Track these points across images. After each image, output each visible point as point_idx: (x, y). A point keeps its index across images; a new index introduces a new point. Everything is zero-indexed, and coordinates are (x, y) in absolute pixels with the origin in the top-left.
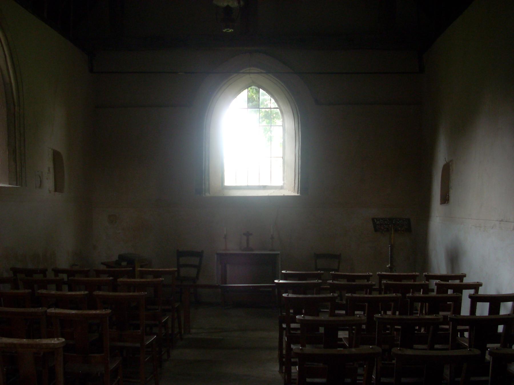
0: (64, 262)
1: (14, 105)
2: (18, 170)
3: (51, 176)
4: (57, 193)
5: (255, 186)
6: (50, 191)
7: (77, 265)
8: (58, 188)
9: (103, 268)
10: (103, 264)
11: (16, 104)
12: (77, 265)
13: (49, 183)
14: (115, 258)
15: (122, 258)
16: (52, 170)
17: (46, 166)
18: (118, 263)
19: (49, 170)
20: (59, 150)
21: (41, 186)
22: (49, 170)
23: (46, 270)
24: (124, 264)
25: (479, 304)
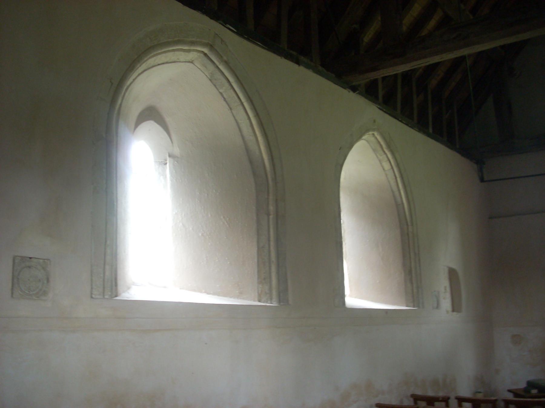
0: (465, 391)
1: (407, 225)
2: (415, 290)
3: (448, 295)
4: (455, 313)
5: (286, 57)
6: (447, 312)
7: (480, 392)
8: (456, 307)
9: (510, 396)
10: (509, 391)
11: (409, 224)
12: (480, 392)
13: (446, 303)
14: (522, 385)
15: (531, 385)
16: (448, 289)
17: (443, 284)
18: (527, 390)
19: (445, 289)
20: (453, 266)
21: (438, 306)
22: (445, 289)
23: (449, 398)
24: (534, 392)
25: (486, 178)
